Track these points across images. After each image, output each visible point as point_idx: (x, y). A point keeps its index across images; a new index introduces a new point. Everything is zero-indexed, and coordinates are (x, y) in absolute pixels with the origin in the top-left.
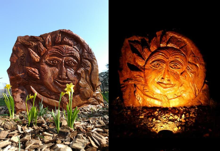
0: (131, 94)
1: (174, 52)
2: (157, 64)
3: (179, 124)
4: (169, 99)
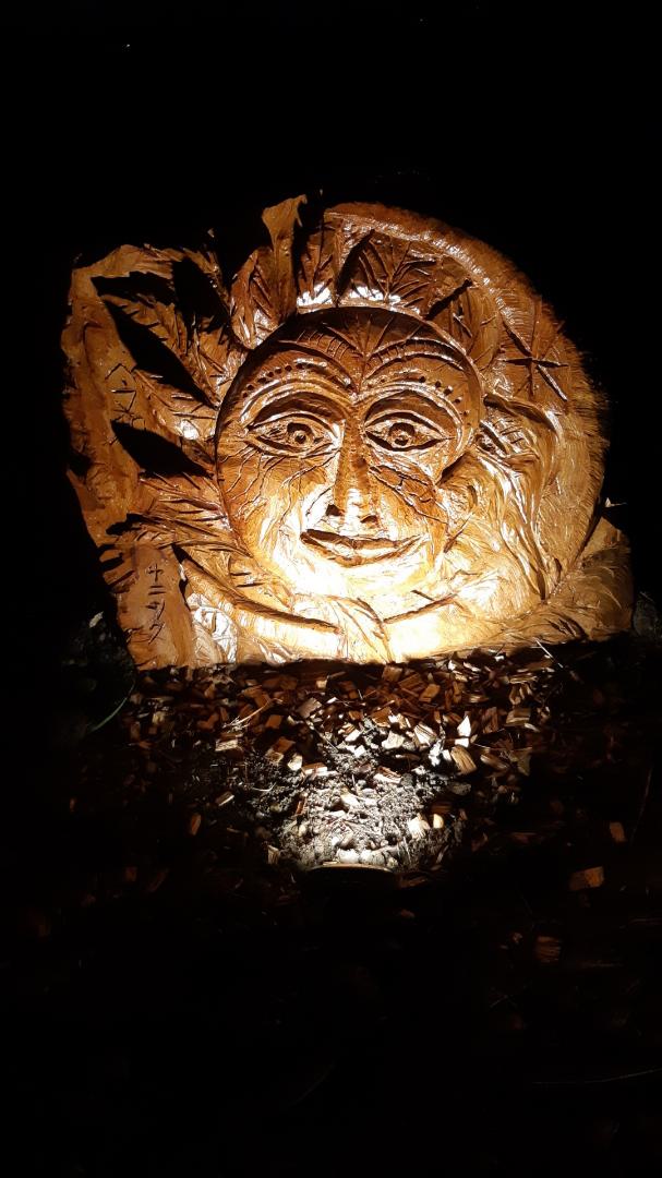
0: (161, 599)
1: (392, 343)
2: (292, 428)
3: (438, 789)
4: (385, 620)
